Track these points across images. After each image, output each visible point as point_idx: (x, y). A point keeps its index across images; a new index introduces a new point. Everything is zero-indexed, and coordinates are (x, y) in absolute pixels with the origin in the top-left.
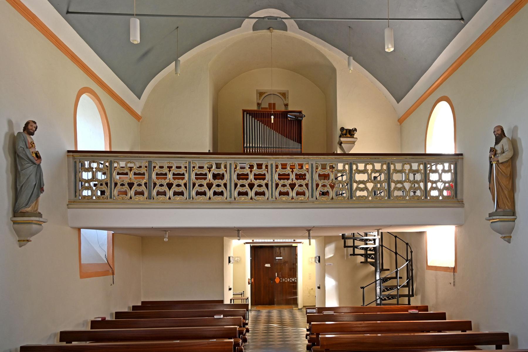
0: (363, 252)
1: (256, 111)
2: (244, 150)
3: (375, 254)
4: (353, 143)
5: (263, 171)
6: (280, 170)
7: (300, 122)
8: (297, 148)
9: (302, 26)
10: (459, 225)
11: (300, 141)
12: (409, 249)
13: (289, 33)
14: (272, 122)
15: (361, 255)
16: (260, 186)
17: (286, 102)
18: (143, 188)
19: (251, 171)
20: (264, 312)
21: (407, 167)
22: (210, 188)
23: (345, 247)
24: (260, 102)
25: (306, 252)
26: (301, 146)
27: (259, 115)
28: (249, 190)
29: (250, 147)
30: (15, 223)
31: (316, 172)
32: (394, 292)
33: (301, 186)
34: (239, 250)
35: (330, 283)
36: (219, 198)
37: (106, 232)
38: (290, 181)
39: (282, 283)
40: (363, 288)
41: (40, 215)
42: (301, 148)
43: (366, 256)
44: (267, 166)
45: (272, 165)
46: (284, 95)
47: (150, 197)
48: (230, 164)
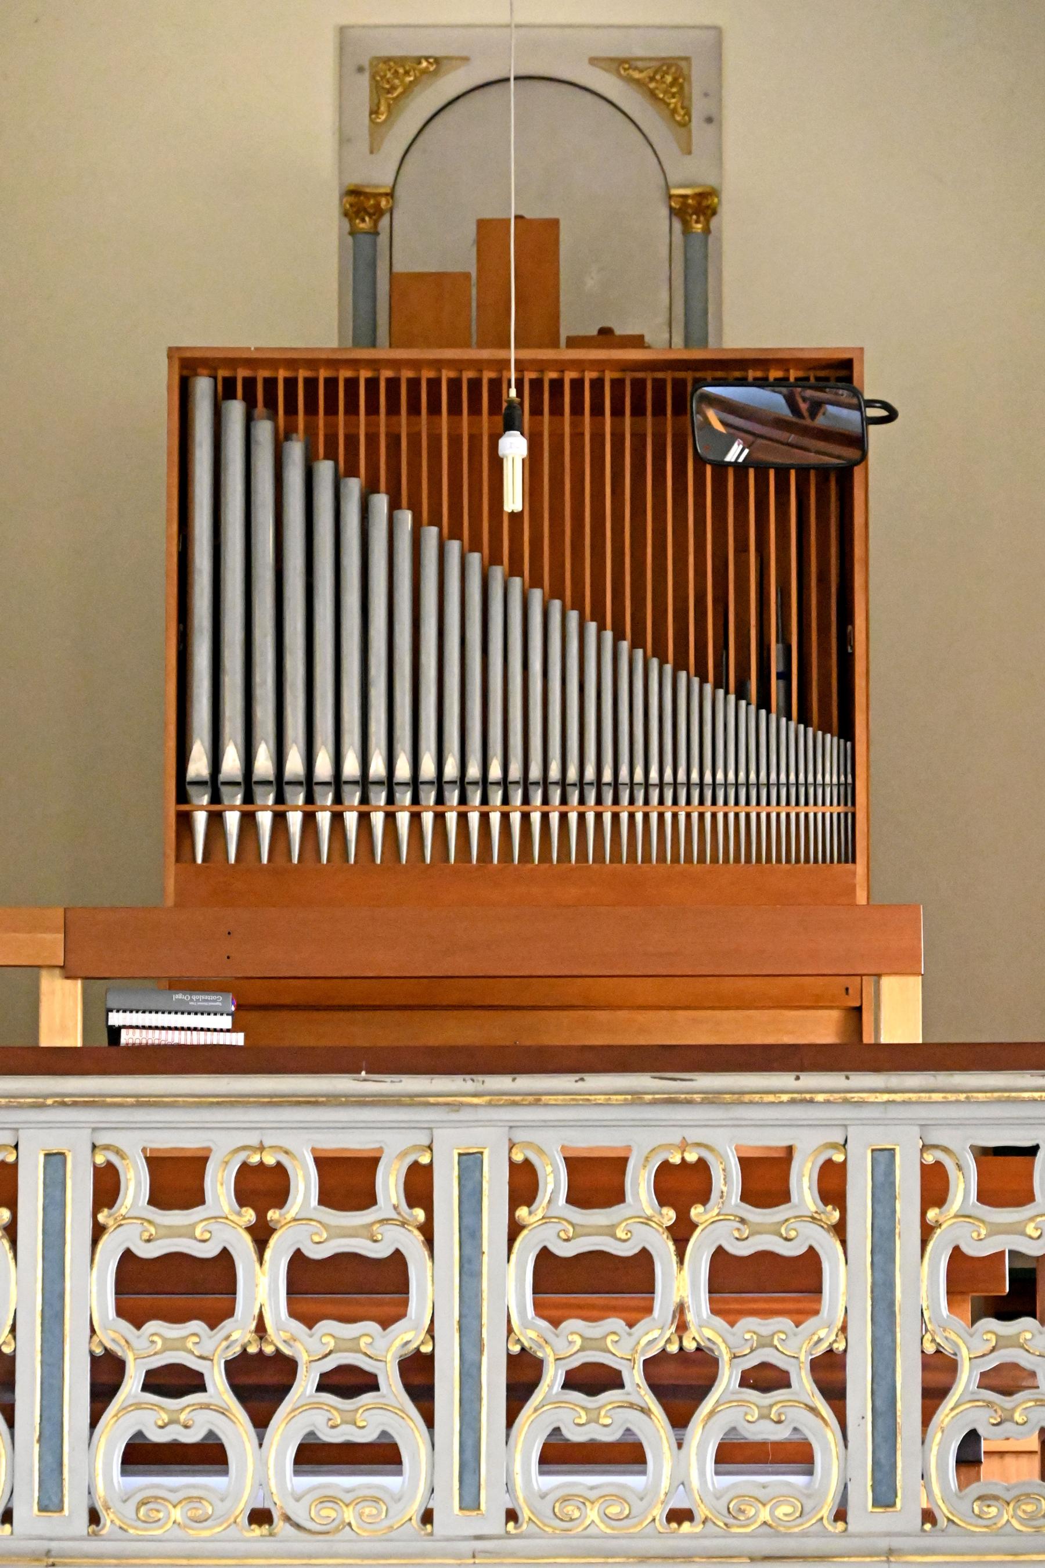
2: (185, 821)
5: (379, 1230)
8: (802, 793)
11: (833, 708)
14: (514, 500)
16: (348, 1383)
17: (688, 174)
19: (261, 1235)
26: (849, 763)
28: (235, 1427)
29: (248, 782)
31: (927, 1231)
33: (765, 1379)
38: (654, 1335)
42: (848, 794)
44: (419, 1187)
45: (470, 1164)
46: (668, 84)
48: (55, 1160)
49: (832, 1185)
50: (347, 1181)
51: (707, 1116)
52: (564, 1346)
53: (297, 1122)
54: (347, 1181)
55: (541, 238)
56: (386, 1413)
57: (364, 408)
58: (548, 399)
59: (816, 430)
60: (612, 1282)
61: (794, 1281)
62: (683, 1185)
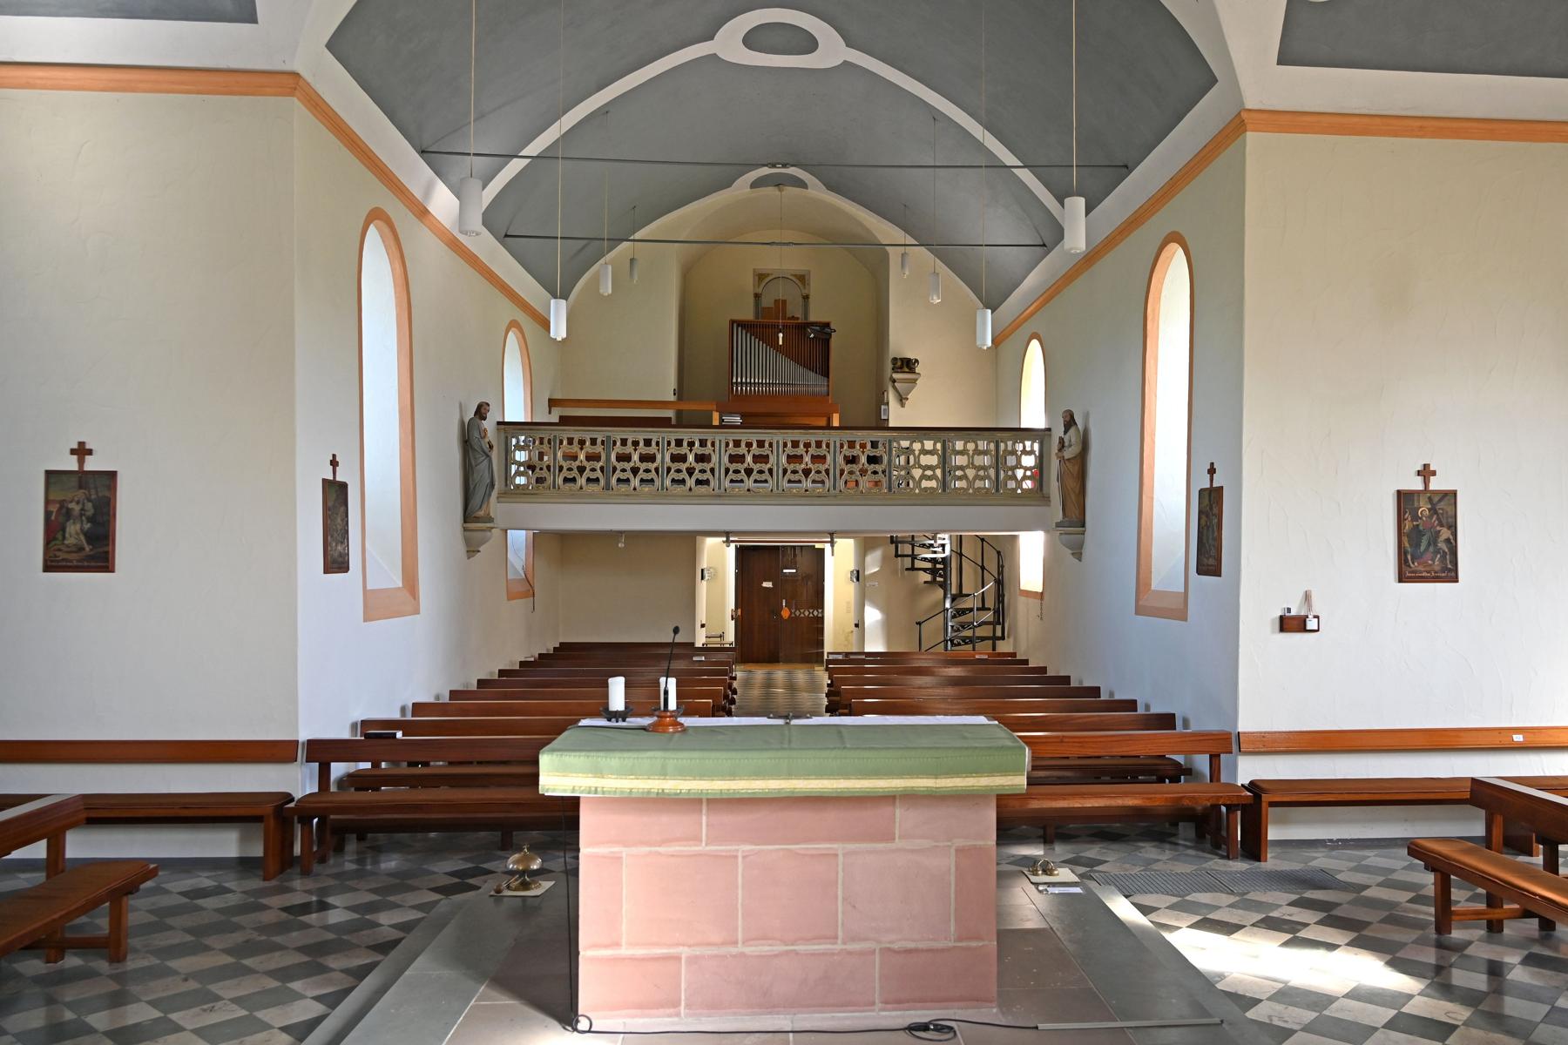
0: (929, 565)
3: (944, 569)
4: (914, 381)
5: (765, 451)
6: (790, 450)
7: (827, 342)
9: (830, 187)
10: (1047, 531)
11: (826, 373)
12: (997, 561)
13: (811, 192)
15: (925, 570)
16: (761, 472)
17: (805, 292)
18: (598, 474)
20: (760, 673)
21: (971, 446)
22: (692, 476)
23: (897, 556)
24: (759, 291)
25: (840, 560)
30: (465, 530)
32: (968, 633)
33: (818, 472)
34: (719, 558)
35: (873, 615)
36: (703, 489)
37: (523, 532)
39: (792, 619)
40: (919, 623)
41: (491, 520)
43: (933, 572)
44: (771, 445)
46: (802, 279)
47: (608, 487)
49: (828, 446)
50: (874, 445)
52: (791, 467)
53: (753, 436)
54: (648, 443)
55: (784, 302)
56: (766, 476)
57: (759, 328)
58: (785, 329)
59: (825, 330)
60: (799, 458)
61: (652, 458)
62: (582, 443)
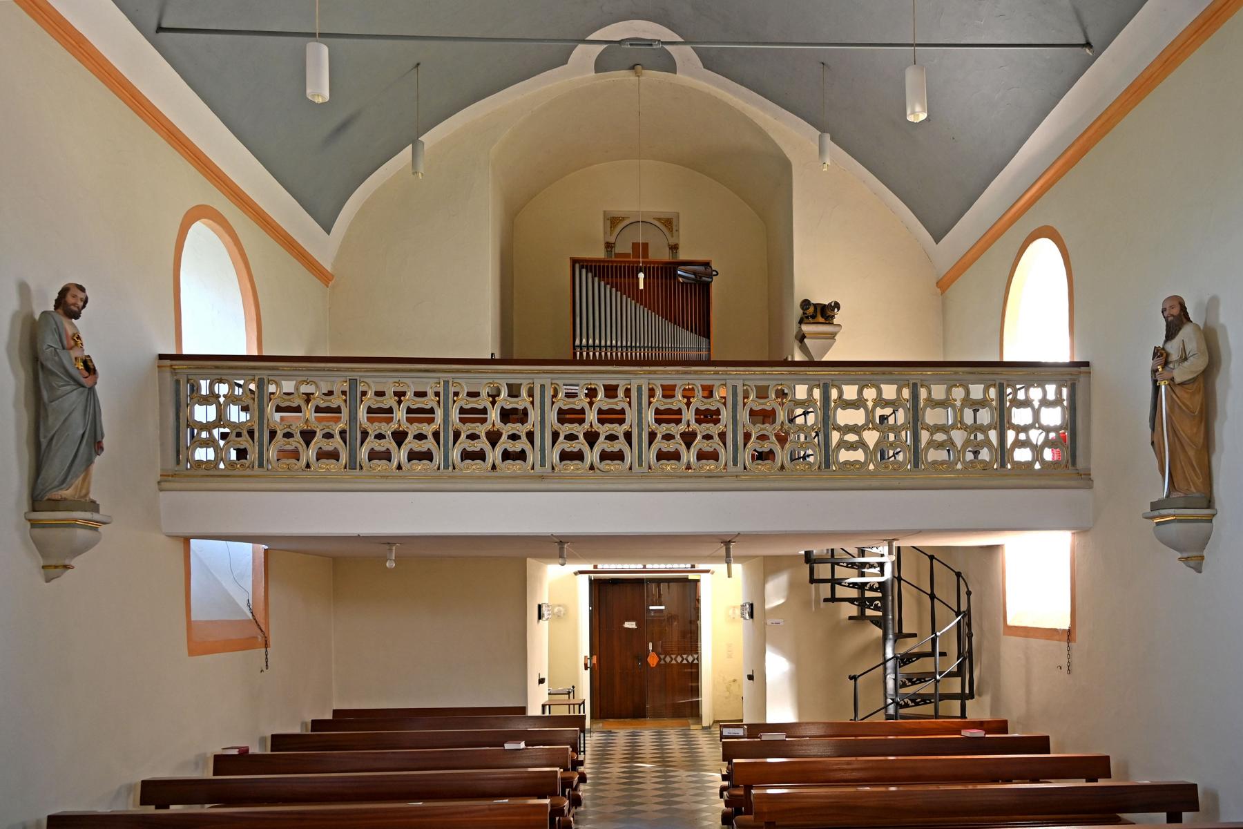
0: (854, 593)
1: (604, 261)
2: (575, 354)
3: (883, 599)
4: (832, 336)
5: (619, 403)
6: (659, 401)
7: (706, 287)
8: (699, 349)
9: (710, 62)
10: (1081, 530)
11: (706, 333)
12: (963, 587)
13: (681, 77)
14: (641, 287)
15: (851, 600)
16: (612, 438)
17: (672, 241)
18: (337, 442)
19: (591, 404)
20: (621, 734)
21: (958, 393)
22: (495, 443)
23: (812, 581)
24: (612, 240)
25: (721, 593)
26: (709, 344)
27: (611, 271)
28: (586, 448)
29: (588, 346)
30: (34, 524)
31: (745, 404)
32: (927, 688)
33: (708, 437)
34: (563, 588)
35: (777, 666)
36: (515, 466)
37: (248, 546)
38: (682, 427)
39: (663, 668)
40: (854, 678)
41: (94, 506)
42: (709, 350)
43: (862, 602)
44: (628, 392)
45: (639, 388)
46: (669, 223)
47: (353, 464)
48: (543, 386)
50: (611, 391)
51: (619, 567)
